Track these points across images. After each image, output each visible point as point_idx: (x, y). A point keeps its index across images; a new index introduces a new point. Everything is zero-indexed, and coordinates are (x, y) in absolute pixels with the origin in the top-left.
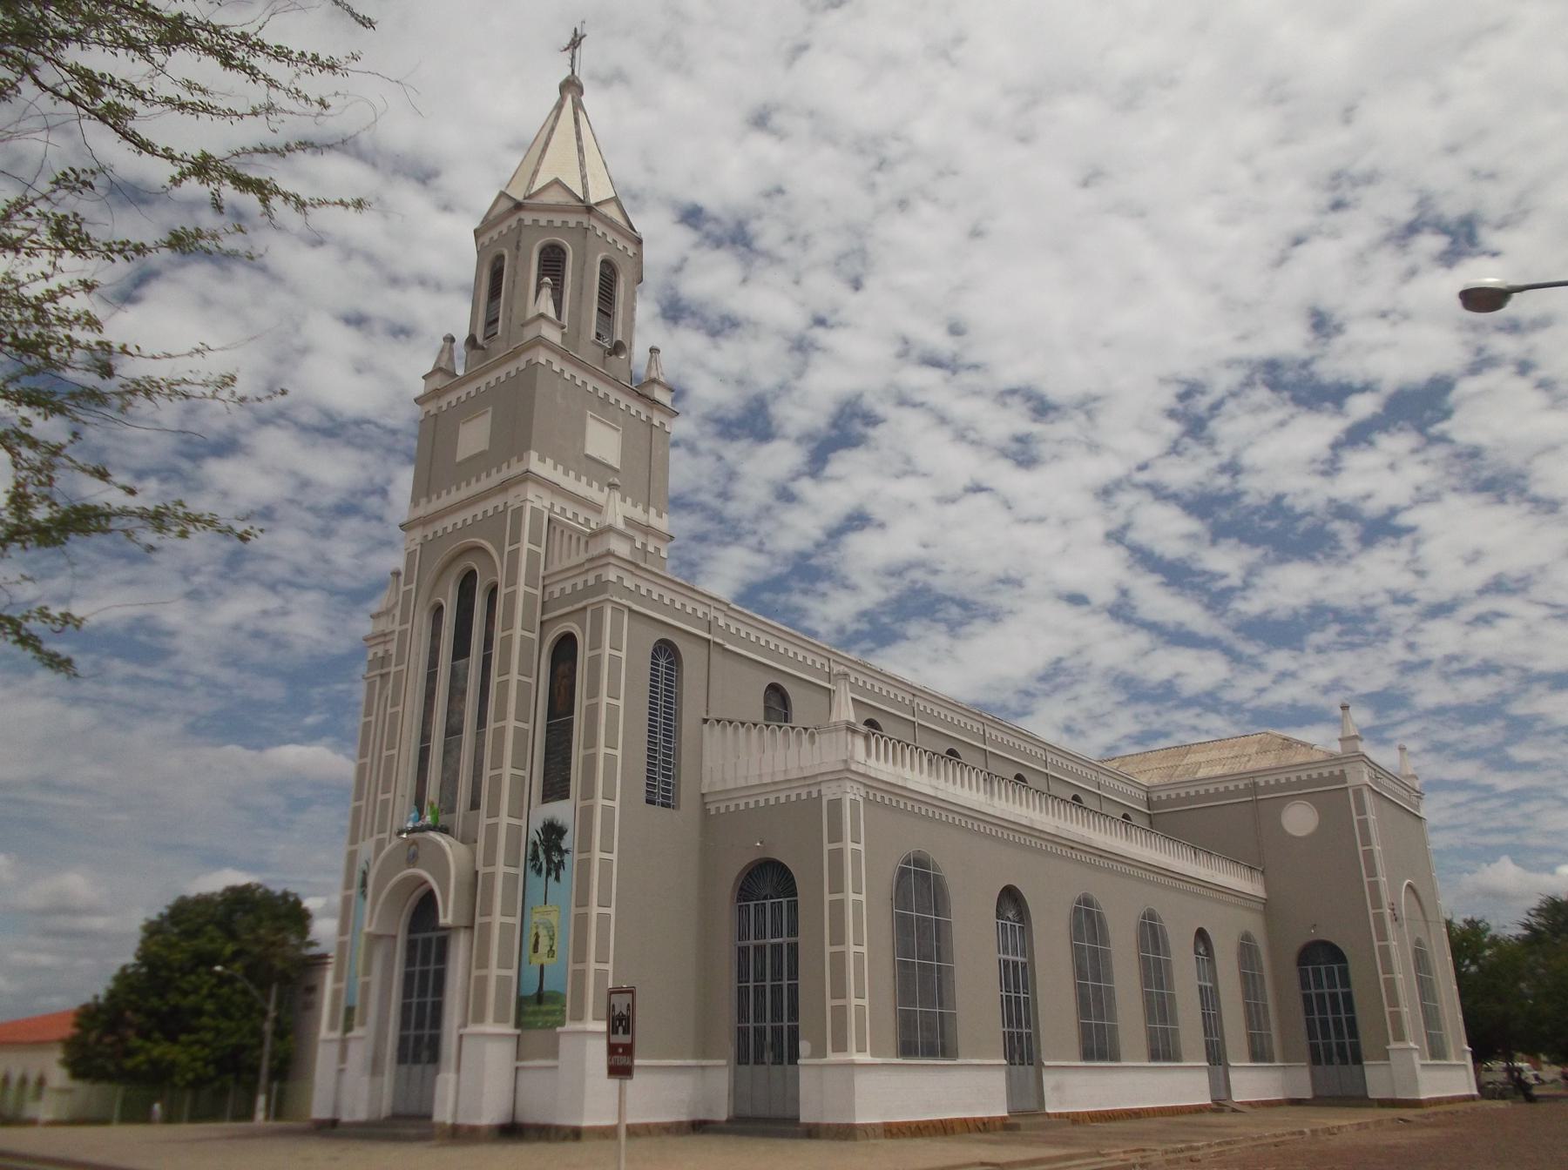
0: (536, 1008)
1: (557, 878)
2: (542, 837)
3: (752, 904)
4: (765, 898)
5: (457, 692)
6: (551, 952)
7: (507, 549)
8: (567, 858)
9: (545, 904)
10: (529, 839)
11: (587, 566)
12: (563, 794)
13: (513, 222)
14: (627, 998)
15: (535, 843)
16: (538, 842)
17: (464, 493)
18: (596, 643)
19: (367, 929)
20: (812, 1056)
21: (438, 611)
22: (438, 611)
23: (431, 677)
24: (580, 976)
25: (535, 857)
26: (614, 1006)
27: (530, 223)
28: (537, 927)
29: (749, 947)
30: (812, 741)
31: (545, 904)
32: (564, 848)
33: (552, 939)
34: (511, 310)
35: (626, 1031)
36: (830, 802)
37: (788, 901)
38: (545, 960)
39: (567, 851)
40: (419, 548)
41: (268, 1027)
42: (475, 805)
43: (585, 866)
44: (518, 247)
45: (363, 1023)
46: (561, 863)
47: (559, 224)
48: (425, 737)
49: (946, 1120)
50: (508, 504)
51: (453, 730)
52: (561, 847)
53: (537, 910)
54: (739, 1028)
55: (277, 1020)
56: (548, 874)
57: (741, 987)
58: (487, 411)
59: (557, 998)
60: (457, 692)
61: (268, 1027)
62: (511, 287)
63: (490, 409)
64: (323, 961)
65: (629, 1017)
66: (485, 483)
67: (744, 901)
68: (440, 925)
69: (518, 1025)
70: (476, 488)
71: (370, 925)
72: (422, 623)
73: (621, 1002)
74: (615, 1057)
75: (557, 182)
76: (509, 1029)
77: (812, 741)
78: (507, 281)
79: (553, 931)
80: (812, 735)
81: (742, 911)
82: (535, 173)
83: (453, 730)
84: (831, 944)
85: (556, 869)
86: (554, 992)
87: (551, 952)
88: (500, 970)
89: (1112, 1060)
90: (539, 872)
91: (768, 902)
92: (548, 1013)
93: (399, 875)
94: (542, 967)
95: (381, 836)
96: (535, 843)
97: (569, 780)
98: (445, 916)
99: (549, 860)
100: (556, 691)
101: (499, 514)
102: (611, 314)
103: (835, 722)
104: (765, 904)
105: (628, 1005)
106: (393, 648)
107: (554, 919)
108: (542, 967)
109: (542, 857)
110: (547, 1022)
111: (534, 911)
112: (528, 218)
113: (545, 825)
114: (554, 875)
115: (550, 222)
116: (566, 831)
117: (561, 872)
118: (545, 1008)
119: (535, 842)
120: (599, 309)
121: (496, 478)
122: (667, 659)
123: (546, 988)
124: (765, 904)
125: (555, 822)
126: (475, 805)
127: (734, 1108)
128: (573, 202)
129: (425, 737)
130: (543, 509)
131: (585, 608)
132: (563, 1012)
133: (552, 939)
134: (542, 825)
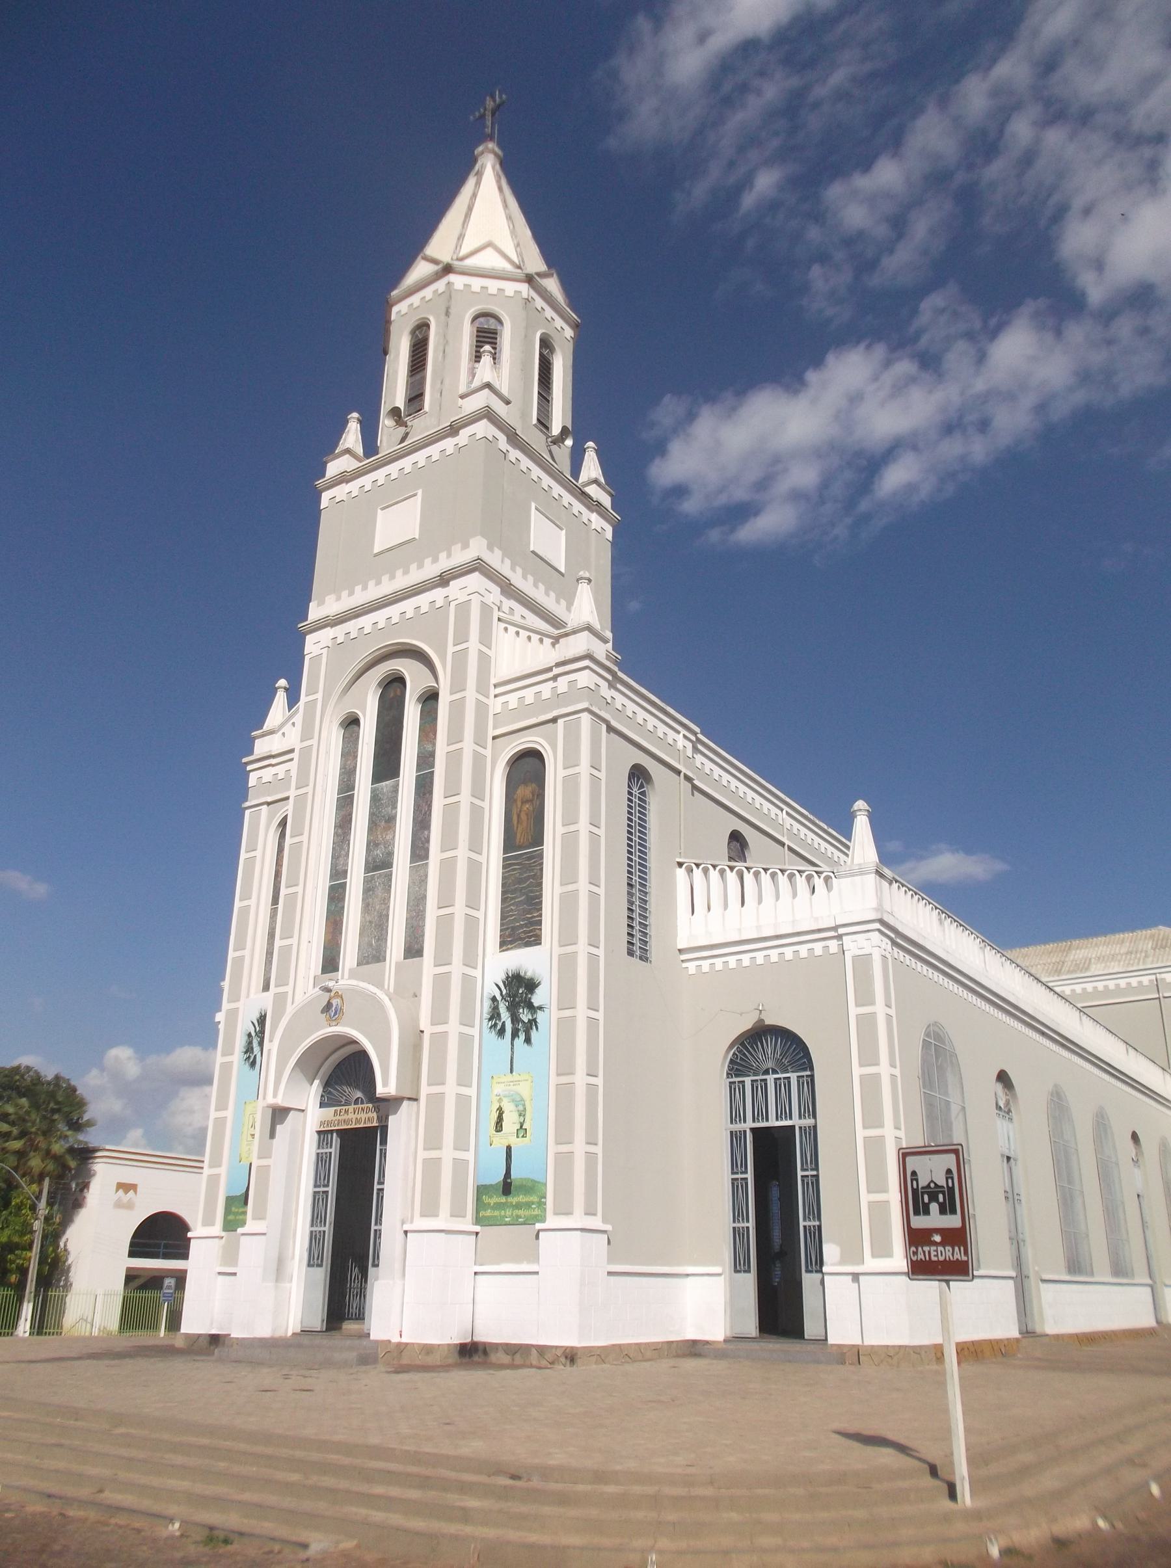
0: (503, 1199)
1: (528, 1040)
2: (504, 992)
3: (748, 1080)
4: (766, 1072)
5: (381, 819)
6: (522, 1130)
7: (451, 649)
8: (540, 1016)
9: (512, 1071)
10: (485, 994)
11: (556, 671)
12: (533, 939)
13: (440, 285)
14: (950, 1161)
15: (494, 999)
16: (499, 998)
17: (387, 587)
18: (571, 760)
19: (270, 1100)
20: (843, 1262)
21: (352, 723)
22: (352, 723)
23: (345, 802)
24: (564, 1161)
25: (495, 1015)
26: (914, 1173)
27: (461, 288)
28: (500, 1100)
29: (745, 1132)
30: (829, 886)
31: (512, 1071)
32: (536, 1004)
33: (522, 1114)
34: (442, 383)
35: (948, 1208)
36: (855, 958)
37: (798, 1077)
38: (514, 1142)
39: (540, 1008)
40: (325, 651)
41: (37, 1225)
42: (414, 950)
43: (566, 1027)
44: (447, 314)
45: (260, 1216)
46: (533, 1022)
47: (494, 292)
48: (338, 873)
49: (624, 1344)
50: (450, 599)
51: (379, 864)
52: (532, 1003)
53: (499, 1080)
54: (734, 1228)
55: (48, 1219)
56: (515, 1034)
57: (737, 1179)
58: (415, 495)
59: (533, 1187)
60: (381, 819)
61: (37, 1225)
62: (440, 358)
63: (420, 492)
64: (90, 1155)
65: (951, 1190)
66: (416, 576)
67: (737, 1076)
68: (377, 1096)
69: (478, 1221)
70: (402, 582)
71: (275, 1095)
72: (333, 737)
73: (932, 1170)
74: (926, 1249)
75: (489, 245)
76: (467, 1224)
77: (829, 886)
78: (435, 351)
79: (524, 1105)
80: (827, 880)
81: (735, 1090)
82: (461, 237)
83: (379, 864)
84: (865, 1127)
85: (525, 1030)
86: (527, 1180)
87: (522, 1130)
88: (426, 1152)
89: (1086, 1274)
90: (501, 1032)
91: (770, 1078)
92: (518, 1206)
93: (313, 1037)
94: (509, 1149)
95: (281, 989)
96: (494, 999)
97: (540, 923)
98: (385, 1084)
99: (515, 1019)
100: (515, 818)
101: (439, 611)
102: (550, 399)
103: (860, 864)
104: (766, 1080)
105: (949, 1171)
106: (293, 766)
107: (524, 1090)
108: (509, 1149)
109: (505, 1016)
110: (518, 1217)
111: (494, 1081)
112: (458, 281)
113: (508, 977)
114: (522, 1036)
115: (484, 288)
116: (539, 984)
117: (534, 1034)
118: (512, 1199)
119: (494, 997)
120: (539, 393)
121: (431, 570)
122: (638, 790)
123: (514, 1174)
124: (766, 1080)
125: (522, 974)
126: (414, 950)
127: (732, 1327)
128: (508, 267)
129: (338, 873)
130: (493, 606)
131: (554, 720)
132: (542, 1204)
133: (522, 1114)
134: (504, 977)
